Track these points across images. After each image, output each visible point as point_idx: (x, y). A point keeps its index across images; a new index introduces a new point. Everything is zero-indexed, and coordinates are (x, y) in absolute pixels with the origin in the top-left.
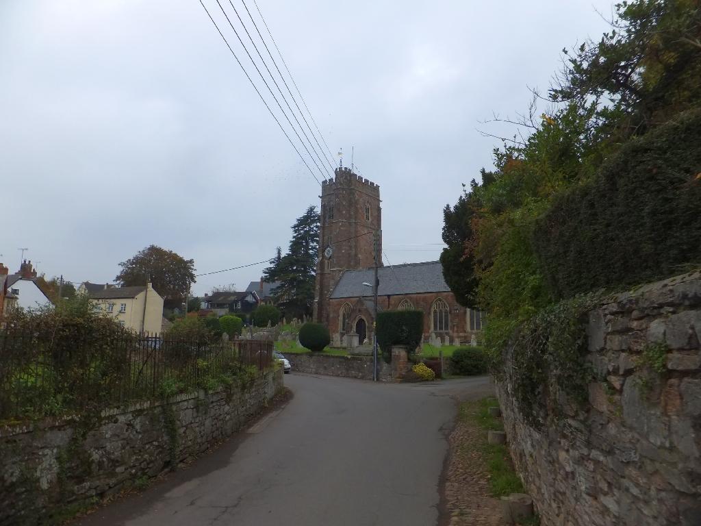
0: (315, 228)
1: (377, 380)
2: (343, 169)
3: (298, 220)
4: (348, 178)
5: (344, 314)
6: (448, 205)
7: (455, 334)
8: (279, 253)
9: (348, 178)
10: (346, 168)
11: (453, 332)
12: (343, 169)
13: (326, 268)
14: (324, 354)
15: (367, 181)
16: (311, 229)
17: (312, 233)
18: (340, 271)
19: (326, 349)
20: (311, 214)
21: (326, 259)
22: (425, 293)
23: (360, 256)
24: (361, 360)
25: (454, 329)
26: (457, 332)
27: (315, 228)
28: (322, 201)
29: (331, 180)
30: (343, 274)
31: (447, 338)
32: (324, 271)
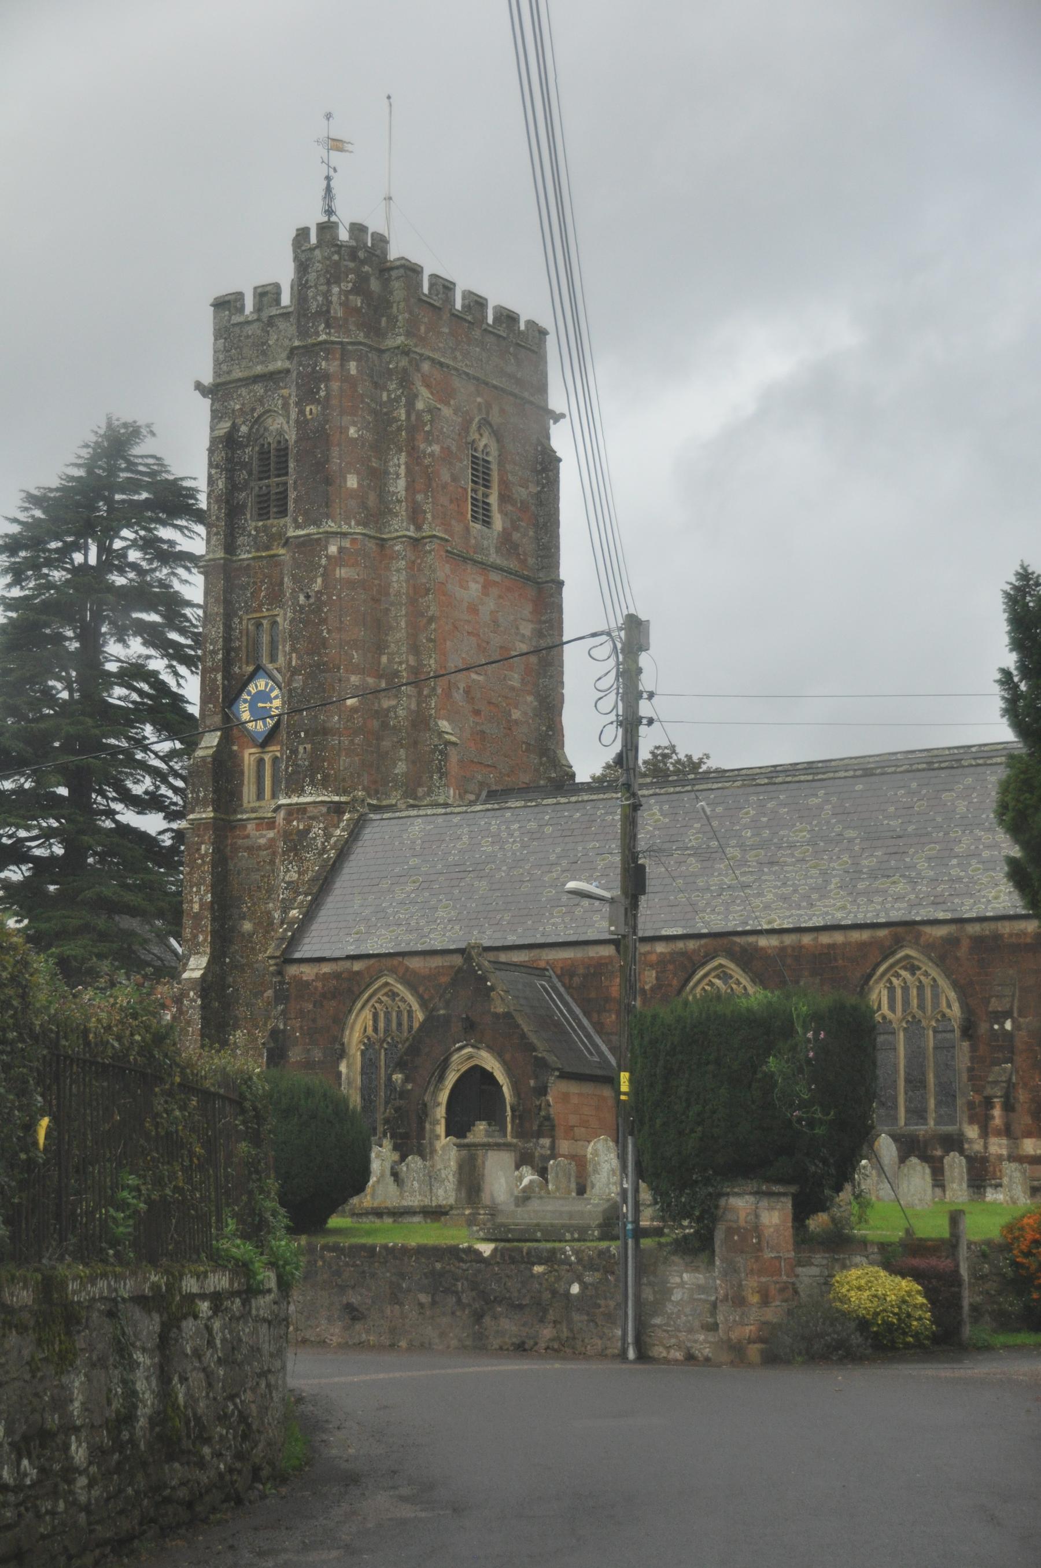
0: (134, 555)
1: (643, 1356)
2: (344, 235)
3: (34, 500)
4: (374, 285)
5: (369, 1046)
6: (93, 431)
7: (998, 1146)
8: (190, 703)
9: (374, 285)
10: (358, 229)
11: (985, 1133)
12: (344, 235)
13: (248, 792)
14: (331, 1240)
15: (476, 303)
16: (112, 560)
17: (120, 581)
18: (337, 809)
19: (334, 1222)
20: (113, 471)
21: (251, 739)
22: (349, 957)
23: (444, 725)
24: (550, 1258)
25: (988, 1118)
26: (1007, 1131)
27: (134, 555)
28: (216, 416)
29: (267, 295)
30: (355, 832)
31: (955, 1165)
32: (238, 808)
